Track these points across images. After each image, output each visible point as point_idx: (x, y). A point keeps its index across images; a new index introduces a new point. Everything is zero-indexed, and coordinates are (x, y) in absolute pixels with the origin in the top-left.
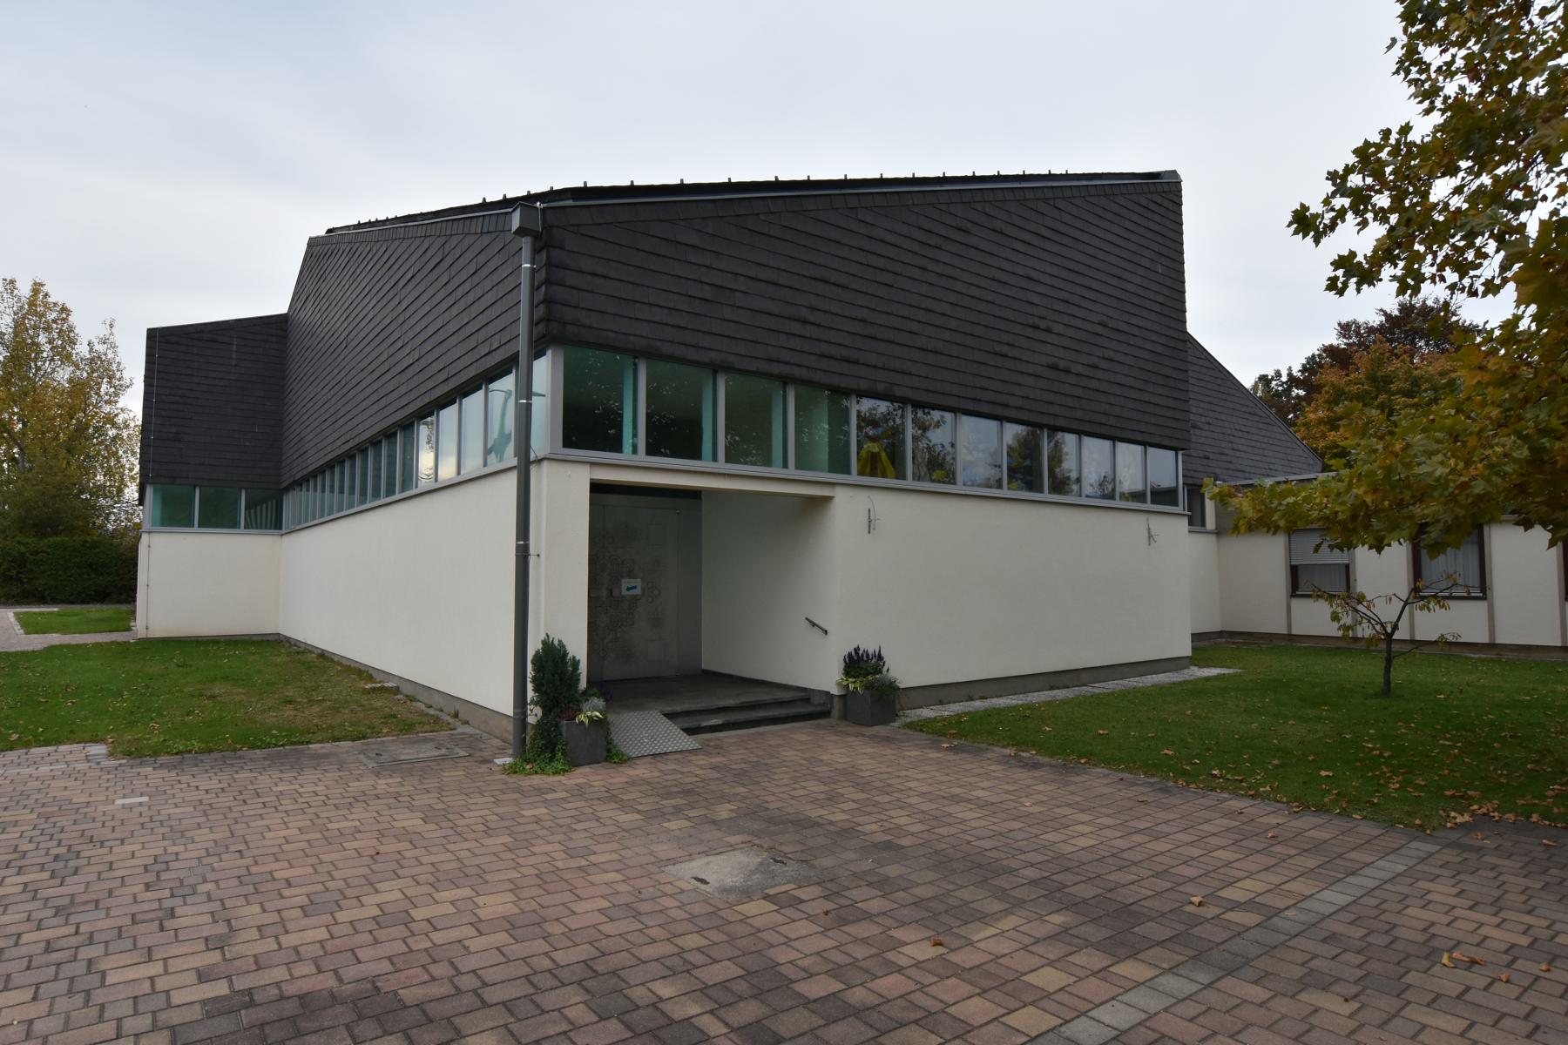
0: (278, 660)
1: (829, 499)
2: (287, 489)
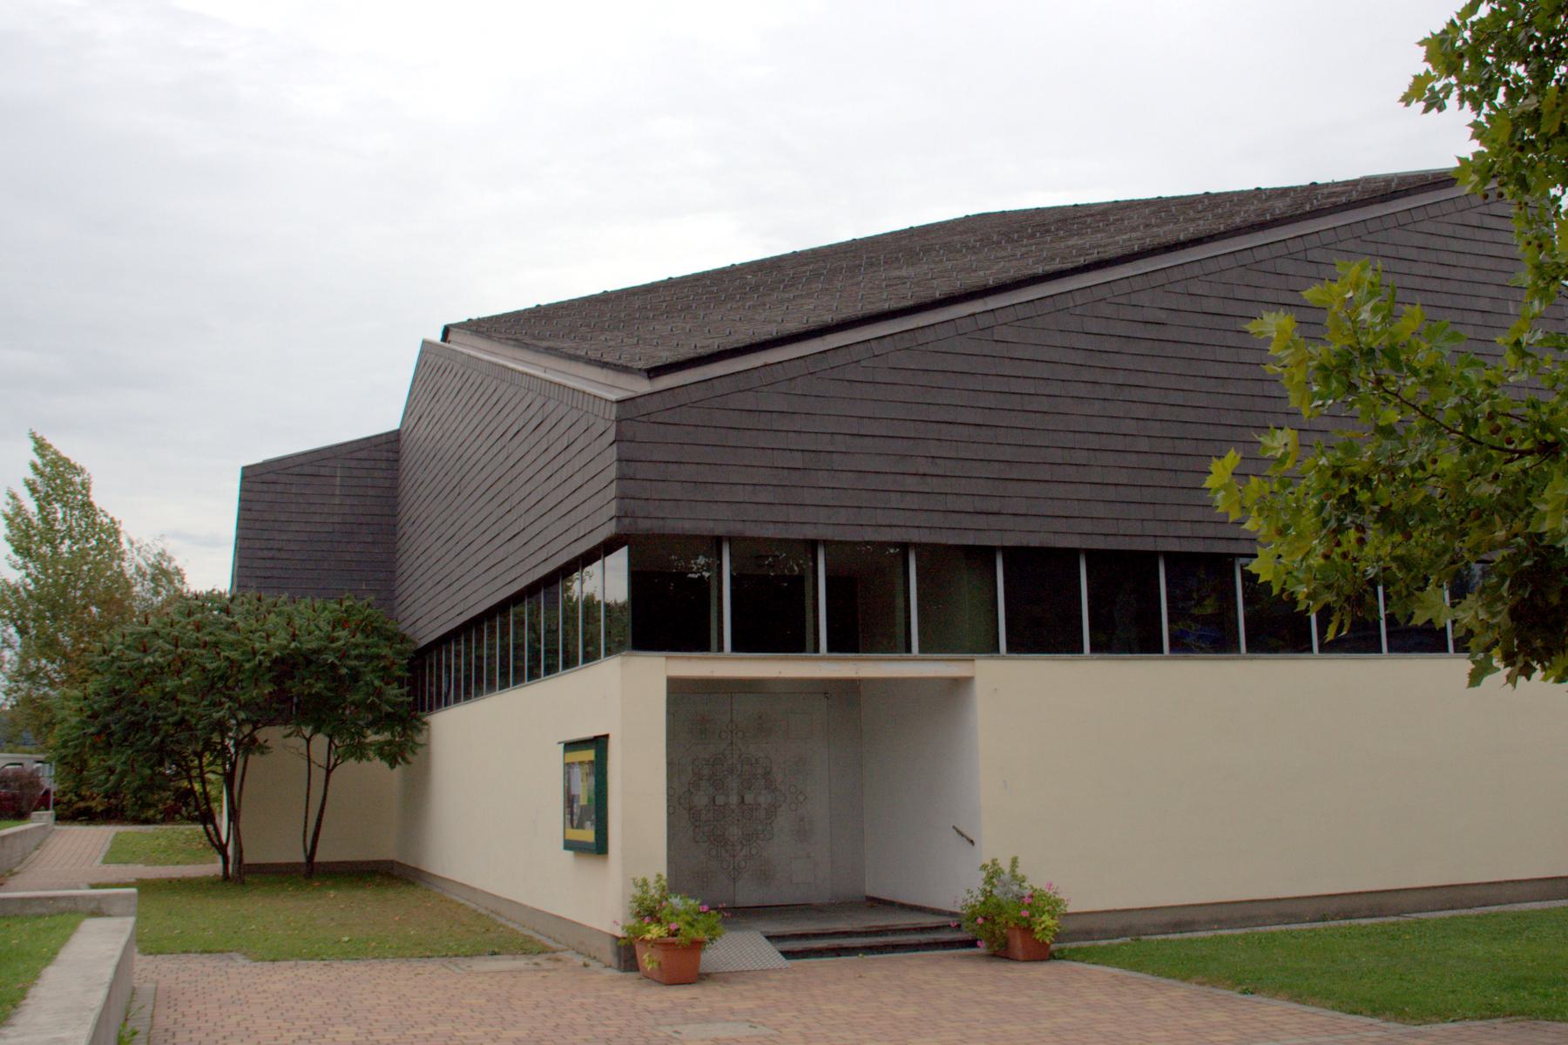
1: (967, 681)
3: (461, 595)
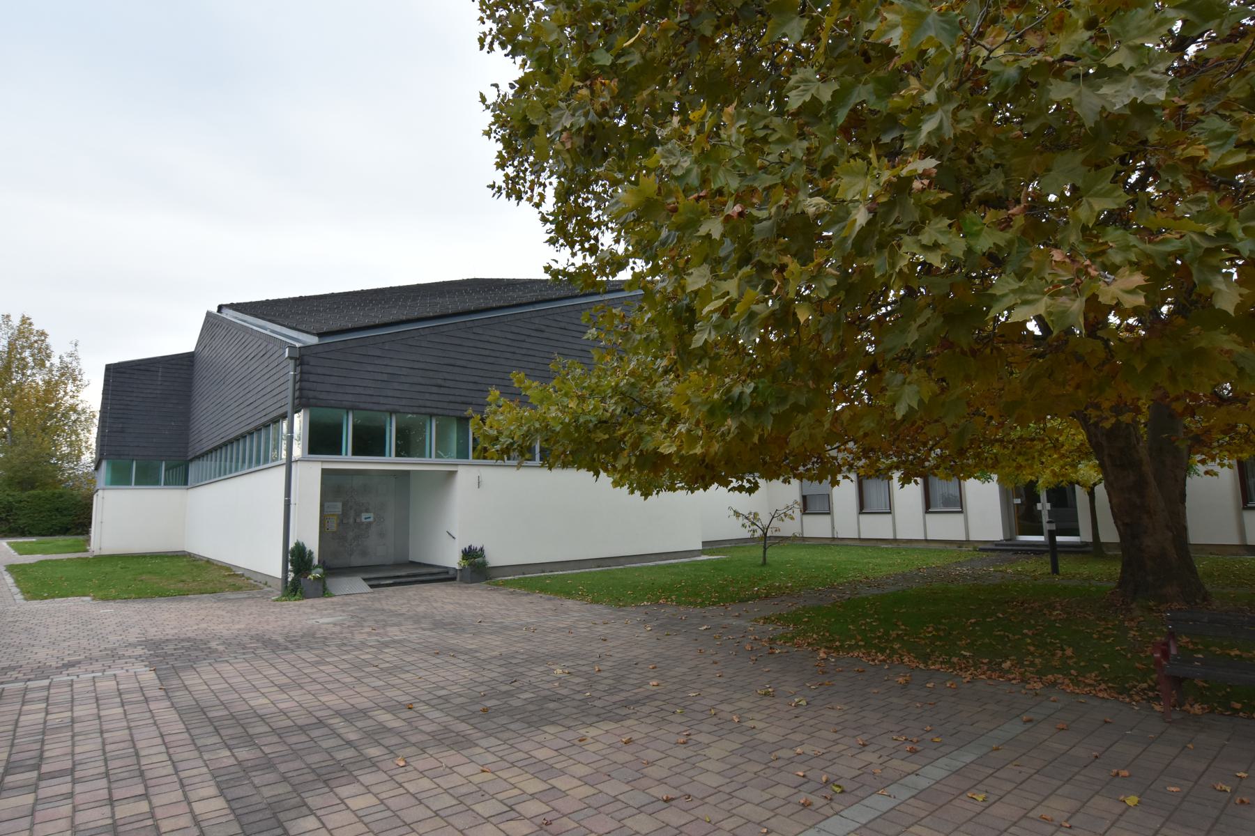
0: (181, 564)
1: (455, 472)
2: (191, 460)
3: (222, 430)
